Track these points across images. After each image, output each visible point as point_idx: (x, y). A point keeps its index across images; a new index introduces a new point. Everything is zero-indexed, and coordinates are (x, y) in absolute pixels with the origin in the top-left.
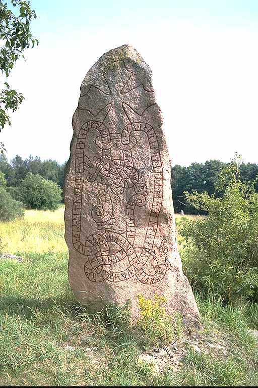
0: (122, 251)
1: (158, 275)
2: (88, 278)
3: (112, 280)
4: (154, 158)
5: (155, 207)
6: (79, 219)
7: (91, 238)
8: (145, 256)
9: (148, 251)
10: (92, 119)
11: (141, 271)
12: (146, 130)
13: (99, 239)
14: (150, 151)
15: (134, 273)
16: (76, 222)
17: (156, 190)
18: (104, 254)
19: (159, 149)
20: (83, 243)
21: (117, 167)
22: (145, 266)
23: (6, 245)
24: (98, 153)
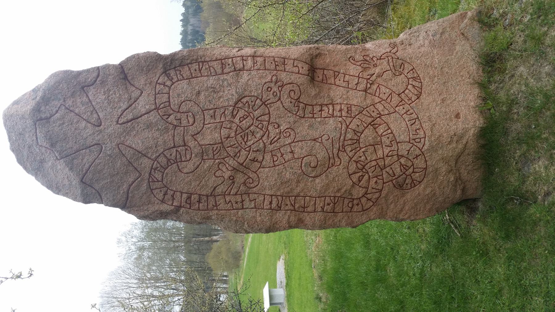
0: (373, 125)
1: (406, 71)
2: (420, 182)
3: (423, 140)
4: (219, 71)
5: (301, 69)
6: (323, 199)
7: (355, 178)
8: (378, 90)
9: (371, 84)
10: (147, 181)
11: (403, 95)
12: (169, 83)
13: (357, 162)
14: (206, 78)
15: (407, 106)
16: (328, 204)
17: (273, 66)
18: (380, 153)
19: (203, 62)
20: (362, 191)
21: (233, 134)
22: (394, 89)
23: (191, 30)
24: (210, 168)
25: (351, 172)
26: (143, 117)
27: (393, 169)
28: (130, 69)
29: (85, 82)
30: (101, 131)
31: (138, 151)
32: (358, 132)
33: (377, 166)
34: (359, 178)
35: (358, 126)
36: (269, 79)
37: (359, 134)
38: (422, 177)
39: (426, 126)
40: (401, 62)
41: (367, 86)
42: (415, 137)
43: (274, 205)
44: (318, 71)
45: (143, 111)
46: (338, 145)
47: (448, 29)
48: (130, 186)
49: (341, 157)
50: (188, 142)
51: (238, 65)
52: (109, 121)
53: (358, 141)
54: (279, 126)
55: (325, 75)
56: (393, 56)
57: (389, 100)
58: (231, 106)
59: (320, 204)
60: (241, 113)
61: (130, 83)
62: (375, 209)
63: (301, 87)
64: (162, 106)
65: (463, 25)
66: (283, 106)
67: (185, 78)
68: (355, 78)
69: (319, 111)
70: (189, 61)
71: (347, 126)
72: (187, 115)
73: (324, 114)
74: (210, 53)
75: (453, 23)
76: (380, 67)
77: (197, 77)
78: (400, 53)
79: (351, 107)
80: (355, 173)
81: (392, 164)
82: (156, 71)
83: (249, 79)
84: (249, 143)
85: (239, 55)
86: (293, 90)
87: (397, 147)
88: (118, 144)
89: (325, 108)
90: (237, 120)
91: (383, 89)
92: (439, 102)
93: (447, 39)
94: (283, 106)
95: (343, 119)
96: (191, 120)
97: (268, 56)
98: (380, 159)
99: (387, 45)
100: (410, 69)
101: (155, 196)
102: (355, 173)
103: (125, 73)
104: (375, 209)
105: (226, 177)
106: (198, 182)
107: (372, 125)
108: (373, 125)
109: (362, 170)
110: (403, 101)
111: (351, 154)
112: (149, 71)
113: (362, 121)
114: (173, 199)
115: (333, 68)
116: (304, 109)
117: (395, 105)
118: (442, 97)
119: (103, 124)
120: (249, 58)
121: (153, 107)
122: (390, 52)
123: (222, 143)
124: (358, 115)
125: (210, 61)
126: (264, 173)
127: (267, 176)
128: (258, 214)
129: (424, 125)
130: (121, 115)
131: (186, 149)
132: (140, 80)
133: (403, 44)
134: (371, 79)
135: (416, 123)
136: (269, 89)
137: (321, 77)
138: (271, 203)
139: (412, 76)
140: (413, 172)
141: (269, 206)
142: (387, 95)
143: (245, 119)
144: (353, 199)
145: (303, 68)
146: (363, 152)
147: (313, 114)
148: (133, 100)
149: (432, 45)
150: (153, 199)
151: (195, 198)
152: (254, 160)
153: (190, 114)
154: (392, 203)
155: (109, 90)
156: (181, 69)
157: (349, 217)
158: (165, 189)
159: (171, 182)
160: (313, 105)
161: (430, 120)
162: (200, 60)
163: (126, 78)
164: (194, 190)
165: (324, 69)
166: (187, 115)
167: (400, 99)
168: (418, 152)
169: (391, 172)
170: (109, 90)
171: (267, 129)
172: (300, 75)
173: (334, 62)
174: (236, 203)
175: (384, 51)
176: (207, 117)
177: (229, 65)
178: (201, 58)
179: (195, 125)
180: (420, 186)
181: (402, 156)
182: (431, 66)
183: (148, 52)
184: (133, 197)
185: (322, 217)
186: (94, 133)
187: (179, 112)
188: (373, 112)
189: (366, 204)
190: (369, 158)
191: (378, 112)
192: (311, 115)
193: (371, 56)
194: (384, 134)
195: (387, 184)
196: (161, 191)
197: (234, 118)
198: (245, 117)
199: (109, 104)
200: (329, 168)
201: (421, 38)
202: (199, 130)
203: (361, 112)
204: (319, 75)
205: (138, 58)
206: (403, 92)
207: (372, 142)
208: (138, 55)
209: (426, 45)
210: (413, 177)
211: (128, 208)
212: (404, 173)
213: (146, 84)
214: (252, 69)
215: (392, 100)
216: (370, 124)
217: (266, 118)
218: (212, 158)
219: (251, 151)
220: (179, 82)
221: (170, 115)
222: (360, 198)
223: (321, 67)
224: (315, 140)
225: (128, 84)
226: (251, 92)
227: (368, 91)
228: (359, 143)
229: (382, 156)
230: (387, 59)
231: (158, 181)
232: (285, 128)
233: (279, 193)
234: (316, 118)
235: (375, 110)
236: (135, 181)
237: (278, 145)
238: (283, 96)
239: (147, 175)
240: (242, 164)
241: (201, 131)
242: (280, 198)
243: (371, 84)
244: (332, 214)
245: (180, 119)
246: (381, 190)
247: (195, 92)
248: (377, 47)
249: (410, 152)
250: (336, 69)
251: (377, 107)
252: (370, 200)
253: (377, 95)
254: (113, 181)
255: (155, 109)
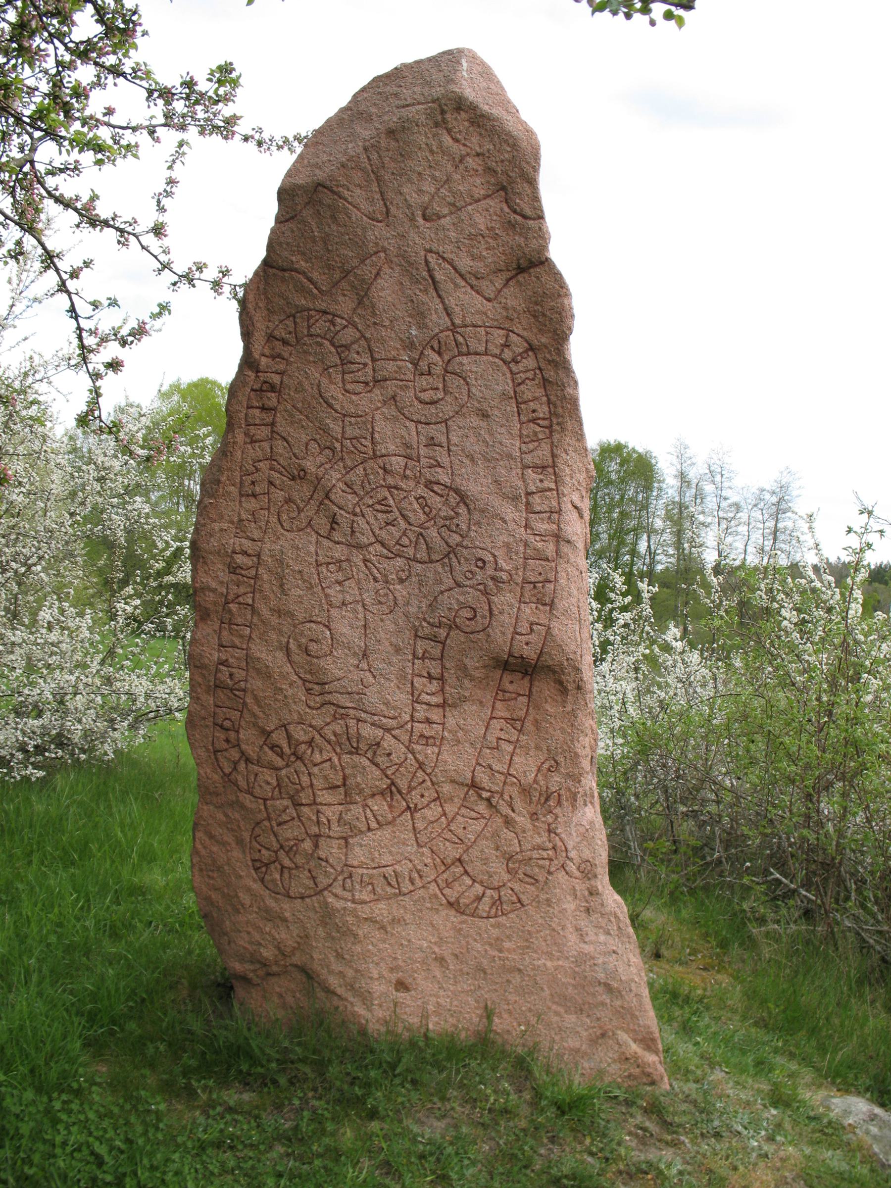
0: (391, 790)
1: (517, 887)
3: (348, 895)
4: (528, 459)
5: (524, 639)
7: (279, 738)
8: (474, 815)
9: (488, 800)
11: (459, 870)
18: (325, 797)
20: (251, 751)
21: (390, 481)
22: (475, 852)
24: (326, 430)
25: (291, 728)
26: (438, 301)
27: (290, 823)
28: (538, 278)
29: (515, 194)
30: (412, 219)
31: (368, 288)
32: (375, 753)
33: (298, 787)
34: (277, 746)
35: (389, 755)
36: (502, 563)
37: (369, 755)
38: (271, 886)
39: (381, 910)
40: (541, 878)
41: (483, 789)
42: (356, 878)
43: (240, 559)
44: (526, 682)
45: (451, 302)
46: (350, 705)
47: (618, 1003)
48: (304, 274)
49: (324, 710)
50: (382, 387)
51: (539, 501)
52: (433, 236)
53: (356, 751)
54: (401, 581)
55: (516, 699)
56: (556, 862)
57: (449, 835)
58: (453, 480)
59: (234, 656)
60: (435, 501)
61: (511, 278)
62: (216, 777)
63: (481, 636)
64: (460, 339)
65: (623, 1036)
66: (442, 592)
67: (517, 389)
68: (506, 767)
69: (428, 673)
70: (553, 398)
71: (388, 730)
72: (437, 389)
73: (419, 682)
74: (569, 445)
75: (633, 1016)
76: (529, 826)
77: (519, 414)
78: (562, 880)
79: (434, 745)
80: (289, 737)
81: (301, 821)
82: (535, 330)
83: (505, 522)
84: (368, 511)
85: (563, 505)
86: (475, 616)
87: (335, 835)
88: (385, 252)
89: (434, 686)
90: (421, 491)
91: (478, 826)
92: (437, 950)
93: (594, 995)
94: (442, 592)
95: (406, 723)
96: (426, 396)
97: (559, 569)
98: (314, 795)
99: (587, 854)
100: (522, 896)
101: (281, 322)
102: (289, 737)
103: (530, 268)
104: (216, 777)
105: (303, 463)
106: (299, 405)
107: (389, 787)
108: (391, 792)
109: (294, 754)
110: (443, 868)
111: (327, 731)
112: (535, 316)
113: (400, 765)
114: (273, 357)
115: (531, 718)
116: (434, 639)
117: (434, 848)
118: (450, 959)
119: (428, 225)
120: (555, 526)
121: (458, 321)
122: (567, 857)
123: (375, 456)
124: (415, 758)
125: (552, 442)
126: (309, 543)
127: (298, 548)
128: (225, 526)
129: (382, 905)
130: (444, 259)
131: (366, 384)
132: (516, 297)
133: (591, 894)
134: (501, 802)
135: (388, 889)
136: (480, 564)
137: (510, 688)
138: (244, 553)
139: (504, 899)
140: (283, 867)
141: (238, 549)
142: (460, 832)
143: (423, 509)
144: (238, 732)
145: (527, 644)
146: (330, 760)
147: (423, 658)
148: (474, 282)
149: (582, 959)
150: (276, 319)
151: (272, 399)
152: (334, 522)
153: (440, 395)
154: (226, 815)
155: (496, 237)
156: (537, 382)
157: (204, 718)
158: (293, 341)
159: (305, 352)
160: (441, 659)
161: (394, 921)
162: (555, 421)
163: (521, 270)
164: (286, 397)
165: (529, 696)
166: (437, 389)
167: (449, 861)
168: (323, 881)
169: (285, 817)
170: (496, 237)
171: (397, 555)
172: (510, 636)
173: (547, 721)
174: (253, 483)
175: (570, 845)
176: (432, 430)
177: (541, 481)
178: (558, 424)
179: (416, 403)
180: (254, 881)
181: (316, 846)
182: (528, 947)
183: (573, 316)
184: (283, 280)
185: (206, 661)
186: (409, 206)
187: (446, 371)
188: (422, 796)
189: (229, 760)
190: (316, 770)
191: (419, 807)
192: (420, 652)
193: (558, 811)
194: (368, 811)
195: (262, 807)
196: (290, 333)
197: (426, 486)
198: (427, 509)
199: (471, 237)
200: (304, 681)
201: (602, 938)
202: (406, 411)
203: (421, 766)
204: (515, 684)
205: (559, 296)
206: (466, 872)
207: (351, 782)
208: (568, 295)
209: (582, 945)
210: (272, 866)
211: (264, 271)
212: (282, 847)
213: (505, 308)
214: (529, 531)
215: (448, 844)
216: (393, 783)
217: (422, 554)
218: (347, 436)
219: (352, 517)
220: (509, 375)
221: (439, 353)
222: (238, 745)
223: (534, 690)
224: (365, 655)
225: (510, 274)
226: (478, 523)
227: (471, 792)
228: (351, 753)
229: (319, 800)
230: (550, 845)
231: (309, 327)
232: (397, 594)
233: (261, 571)
234: (413, 664)
235: (425, 801)
236: (313, 283)
237: (362, 575)
238: (463, 593)
239: (323, 306)
240: (327, 497)
241: (403, 414)
242: (253, 572)
243: (488, 800)
244: (212, 684)
245: (429, 374)
246: (252, 794)
247: (485, 406)
248: (582, 830)
249: (324, 864)
250: (529, 726)
251: (432, 805)
252: (235, 769)
253: (463, 811)
254: (314, 241)
255: (453, 324)
